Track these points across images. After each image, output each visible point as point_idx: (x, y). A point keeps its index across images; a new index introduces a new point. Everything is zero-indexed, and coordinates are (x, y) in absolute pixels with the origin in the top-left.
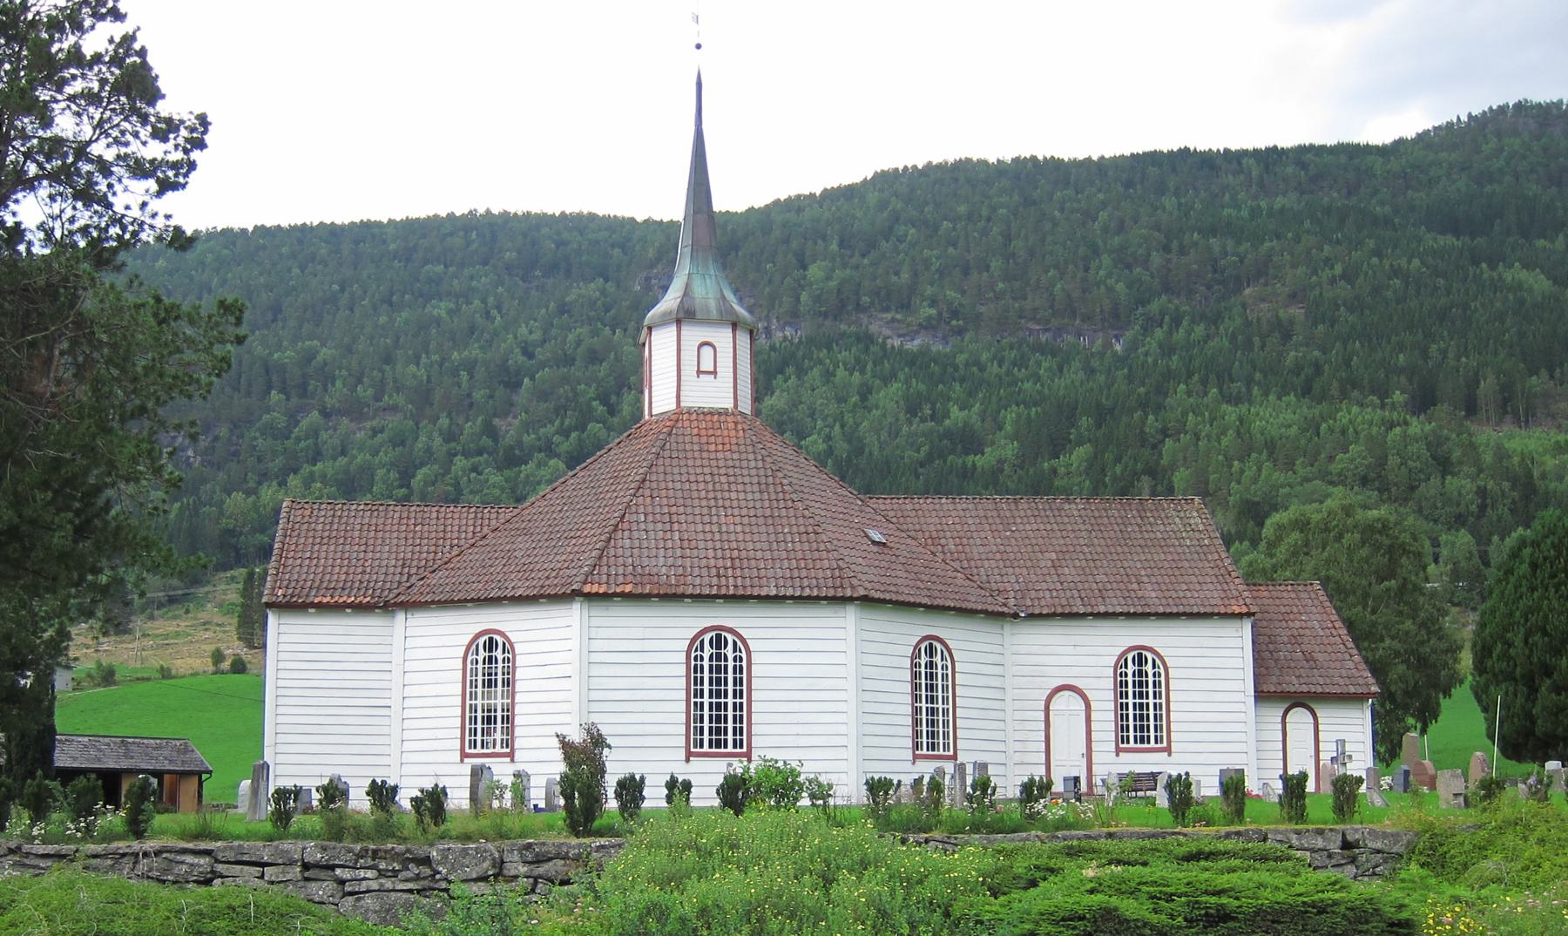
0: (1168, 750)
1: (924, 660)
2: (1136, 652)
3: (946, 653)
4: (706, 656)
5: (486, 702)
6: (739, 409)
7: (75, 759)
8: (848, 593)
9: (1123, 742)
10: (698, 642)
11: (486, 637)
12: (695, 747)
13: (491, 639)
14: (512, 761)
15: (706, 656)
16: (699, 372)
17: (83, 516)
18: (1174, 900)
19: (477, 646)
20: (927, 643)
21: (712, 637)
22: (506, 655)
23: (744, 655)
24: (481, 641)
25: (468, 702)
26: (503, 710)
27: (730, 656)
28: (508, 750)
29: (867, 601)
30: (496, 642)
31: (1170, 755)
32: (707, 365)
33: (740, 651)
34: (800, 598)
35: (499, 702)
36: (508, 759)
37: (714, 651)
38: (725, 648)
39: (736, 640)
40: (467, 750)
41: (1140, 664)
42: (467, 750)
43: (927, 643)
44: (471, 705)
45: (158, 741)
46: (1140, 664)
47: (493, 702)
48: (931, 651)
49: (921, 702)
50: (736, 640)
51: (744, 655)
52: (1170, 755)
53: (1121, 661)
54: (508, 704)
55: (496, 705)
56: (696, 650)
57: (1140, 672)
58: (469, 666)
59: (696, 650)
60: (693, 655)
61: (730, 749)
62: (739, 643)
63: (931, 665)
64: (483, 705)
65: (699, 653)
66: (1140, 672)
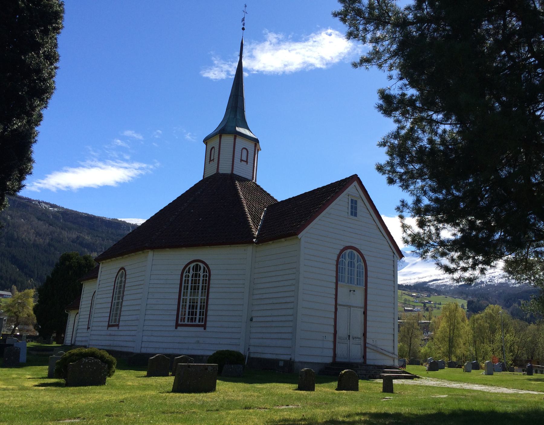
0: (204, 326)
4: (190, 275)
7: (407, 381)
10: (344, 253)
11: (195, 264)
12: (181, 321)
13: (197, 265)
16: (241, 160)
18: (125, 379)
19: (189, 268)
21: (194, 266)
22: (205, 273)
24: (192, 266)
25: (182, 297)
27: (202, 275)
28: (203, 323)
30: (354, 253)
31: (205, 329)
32: (244, 158)
33: (206, 272)
38: (354, 260)
39: (205, 266)
40: (179, 323)
41: (196, 270)
42: (179, 323)
44: (183, 299)
46: (196, 270)
48: (197, 268)
50: (205, 266)
52: (205, 329)
54: (204, 299)
58: (184, 279)
59: (186, 273)
66: (196, 275)
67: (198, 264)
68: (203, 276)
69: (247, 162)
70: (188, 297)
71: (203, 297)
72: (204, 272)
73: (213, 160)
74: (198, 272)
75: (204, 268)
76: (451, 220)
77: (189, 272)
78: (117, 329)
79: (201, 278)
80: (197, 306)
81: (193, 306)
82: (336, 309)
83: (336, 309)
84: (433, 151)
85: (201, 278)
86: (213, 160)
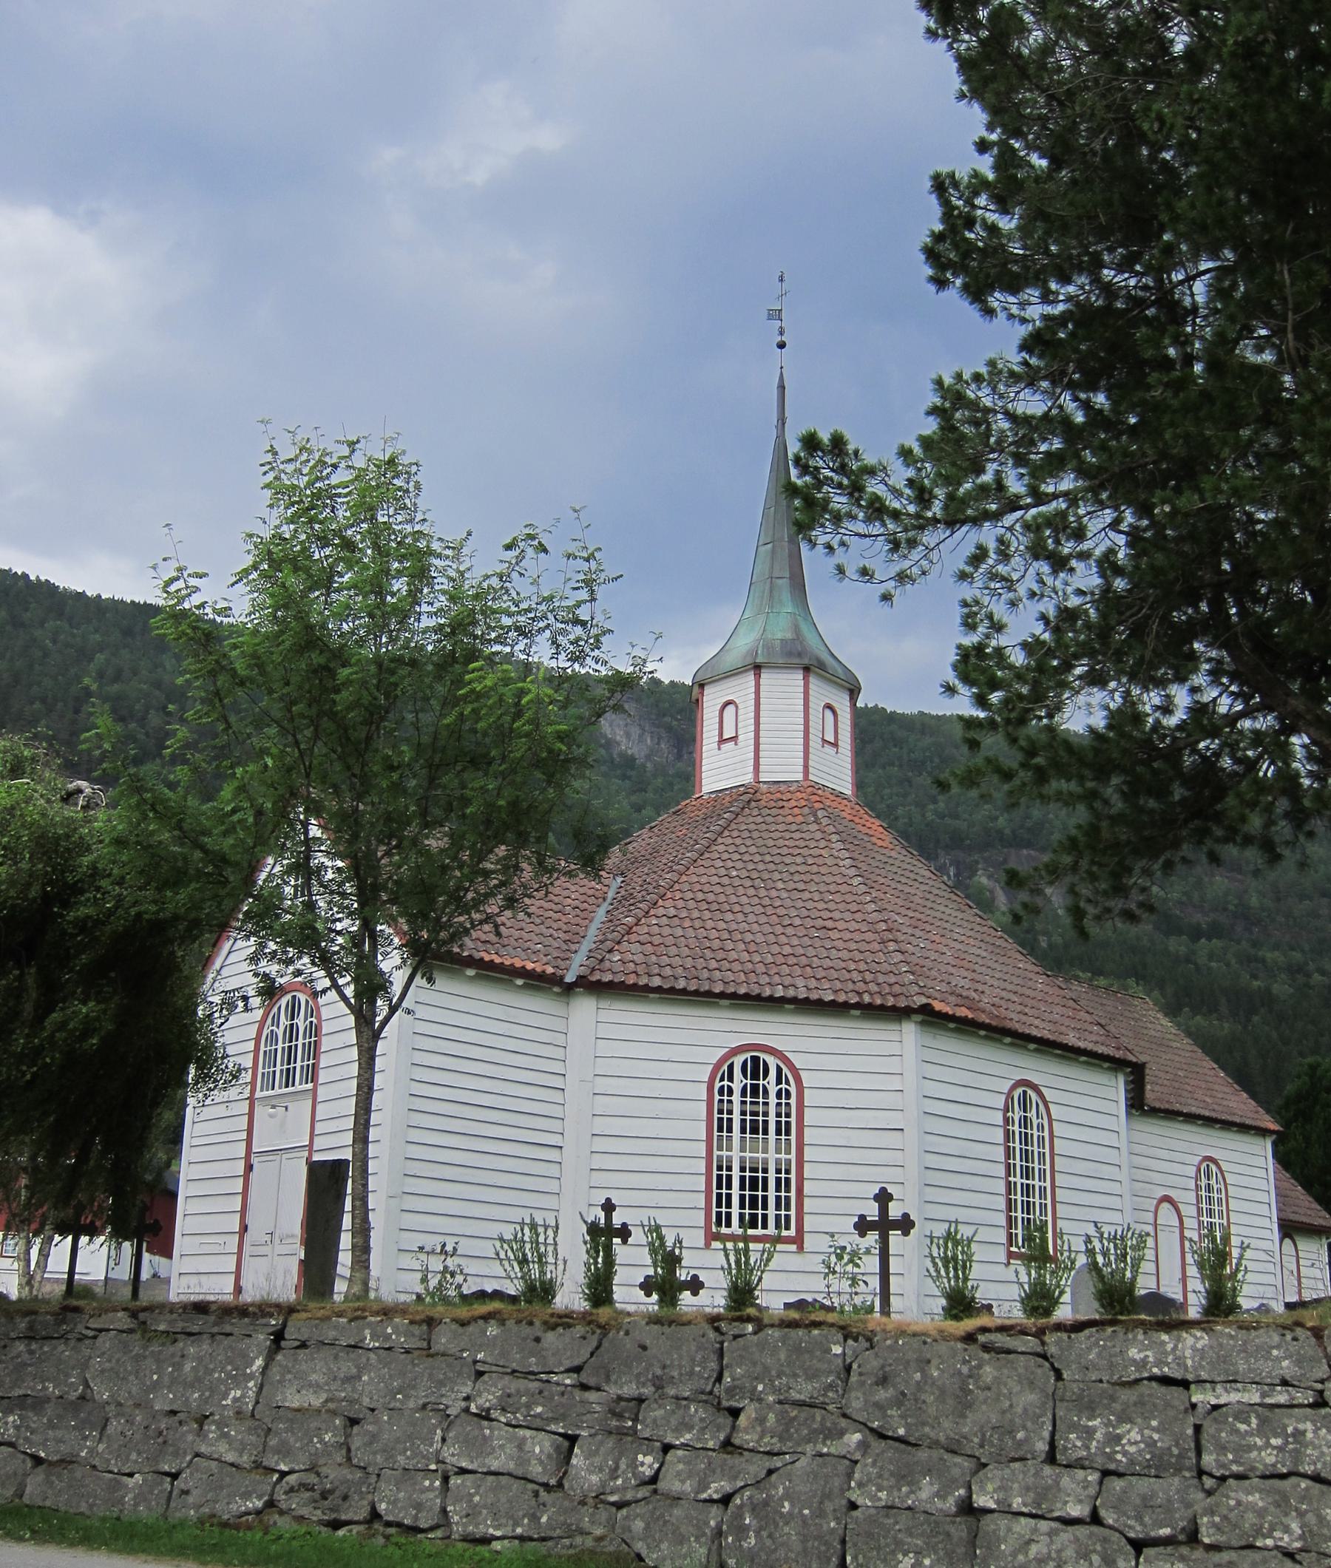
1: (1017, 1115)
2: (748, 1055)
3: (1041, 1106)
4: (737, 1087)
5: (748, 1155)
6: (811, 777)
8: (779, 992)
9: (719, 1224)
14: (801, 1248)
15: (737, 1087)
16: (824, 741)
17: (241, 916)
19: (731, 1067)
20: (1020, 1090)
21: (745, 1063)
22: (783, 1086)
23: (793, 1090)
24: (738, 1061)
26: (778, 1171)
27: (773, 1090)
29: (931, 1017)
33: (787, 1083)
34: (696, 993)
35: (772, 1156)
36: (793, 1247)
37: (761, 1082)
39: (782, 1066)
41: (755, 1076)
43: (1020, 1090)
45: (1189, 1259)
46: (755, 1076)
47: (760, 1155)
48: (755, 1069)
49: (730, 1149)
51: (793, 1090)
53: (723, 1070)
55: (765, 1161)
56: (722, 1079)
57: (755, 1089)
59: (722, 1079)
60: (717, 1085)
61: (771, 1230)
62: (785, 1070)
63: (1025, 1122)
64: (742, 1160)
65: (726, 1083)
66: (755, 1089)
67: (758, 1058)
68: (779, 1095)
69: (835, 745)
70: (736, 1155)
71: (724, 1153)
72: (779, 1082)
73: (734, 739)
74: (761, 1082)
75: (779, 1070)
76: (1193, 651)
77: (731, 1079)
78: (463, 1241)
79: (773, 1100)
80: (765, 1180)
81: (754, 1181)
82: (249, 1167)
83: (249, 1167)
84: (1084, 306)
85: (773, 1100)
86: (734, 739)
